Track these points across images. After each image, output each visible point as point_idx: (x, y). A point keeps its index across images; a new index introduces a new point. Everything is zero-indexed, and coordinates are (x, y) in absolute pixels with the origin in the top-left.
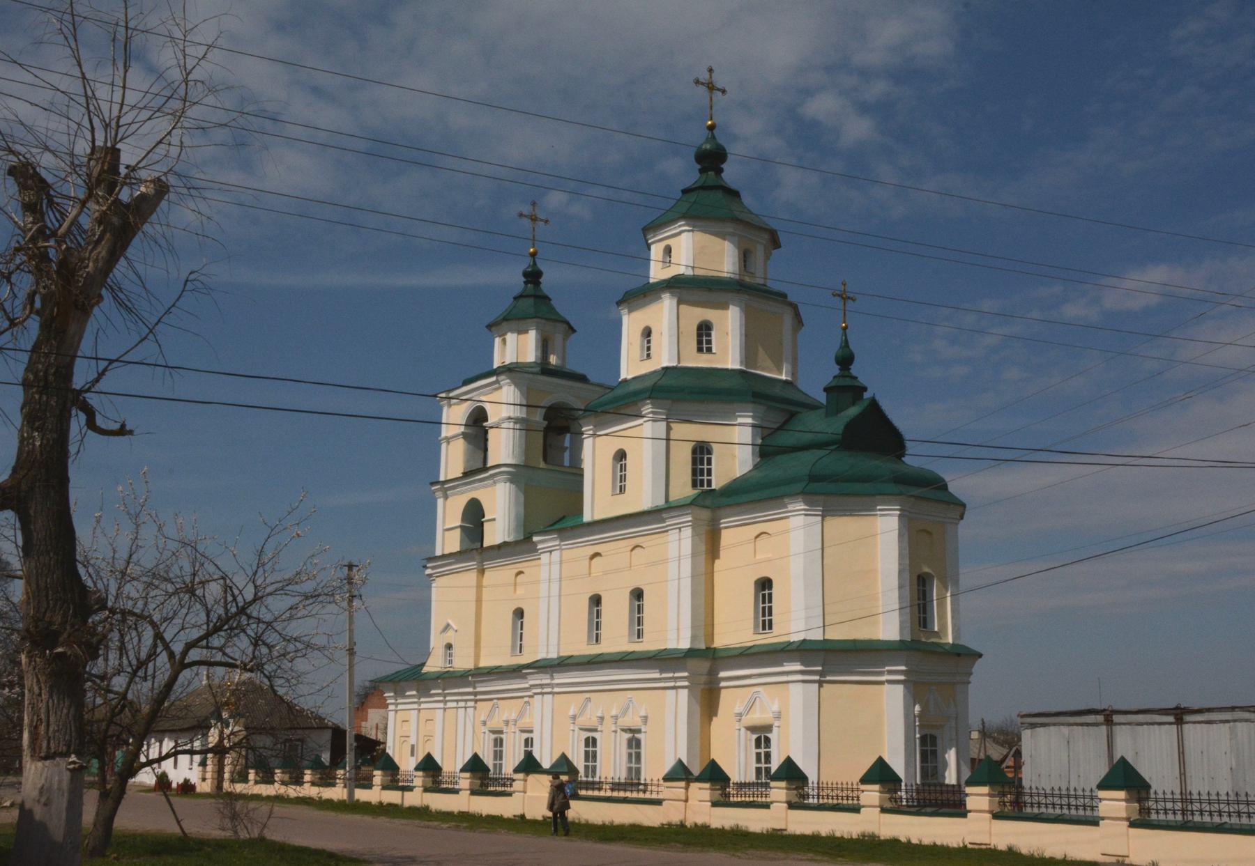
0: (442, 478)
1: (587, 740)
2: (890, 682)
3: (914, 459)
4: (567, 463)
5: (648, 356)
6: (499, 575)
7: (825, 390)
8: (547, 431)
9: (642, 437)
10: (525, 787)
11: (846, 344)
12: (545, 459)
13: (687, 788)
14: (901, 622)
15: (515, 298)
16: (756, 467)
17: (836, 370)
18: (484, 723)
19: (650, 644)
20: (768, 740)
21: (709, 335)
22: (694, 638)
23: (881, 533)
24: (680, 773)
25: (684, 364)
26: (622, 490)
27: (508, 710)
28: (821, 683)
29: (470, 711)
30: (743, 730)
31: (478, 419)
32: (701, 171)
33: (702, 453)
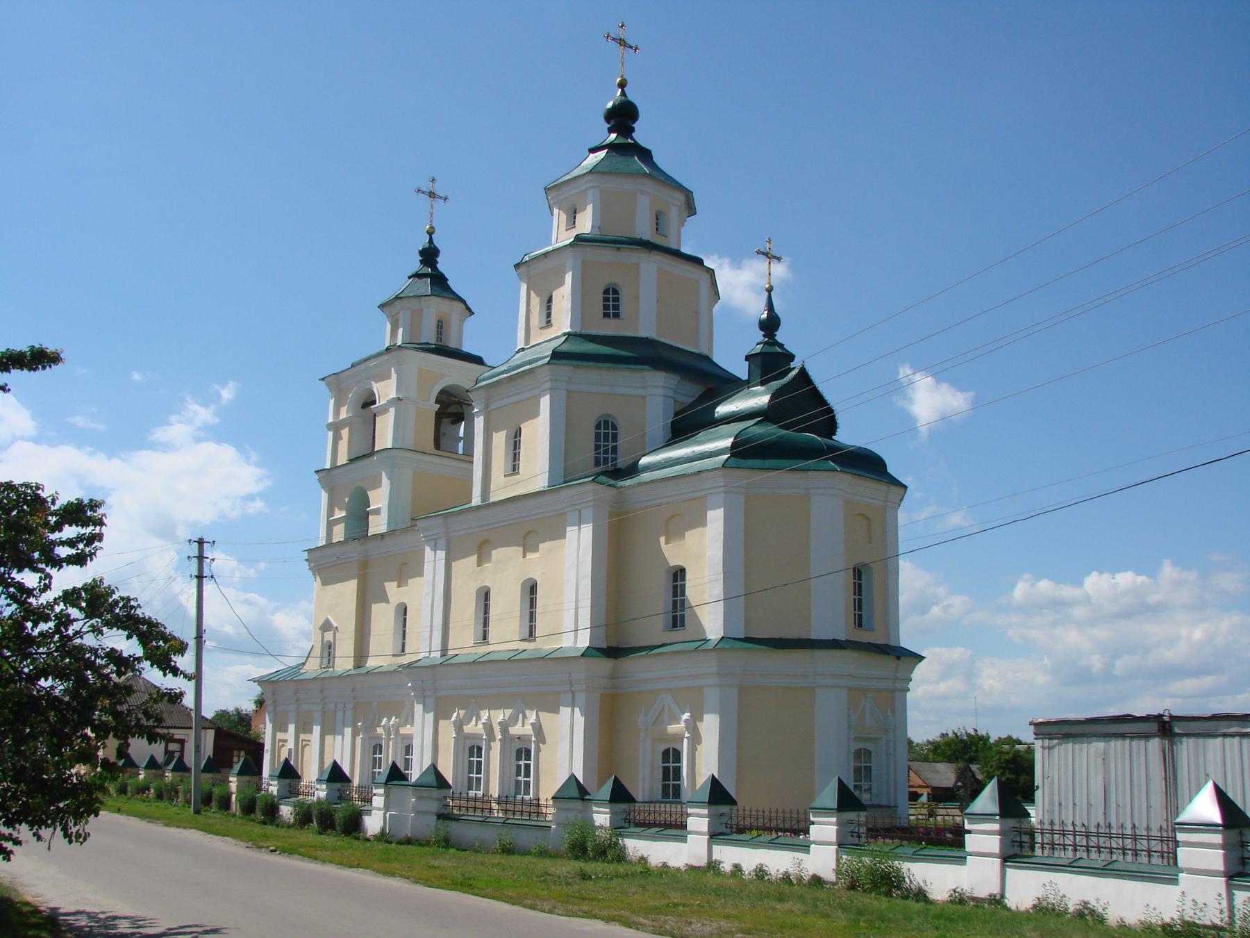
3: (846, 436)
4: (461, 452)
7: (748, 358)
8: (439, 416)
17: (760, 336)
33: (606, 428)
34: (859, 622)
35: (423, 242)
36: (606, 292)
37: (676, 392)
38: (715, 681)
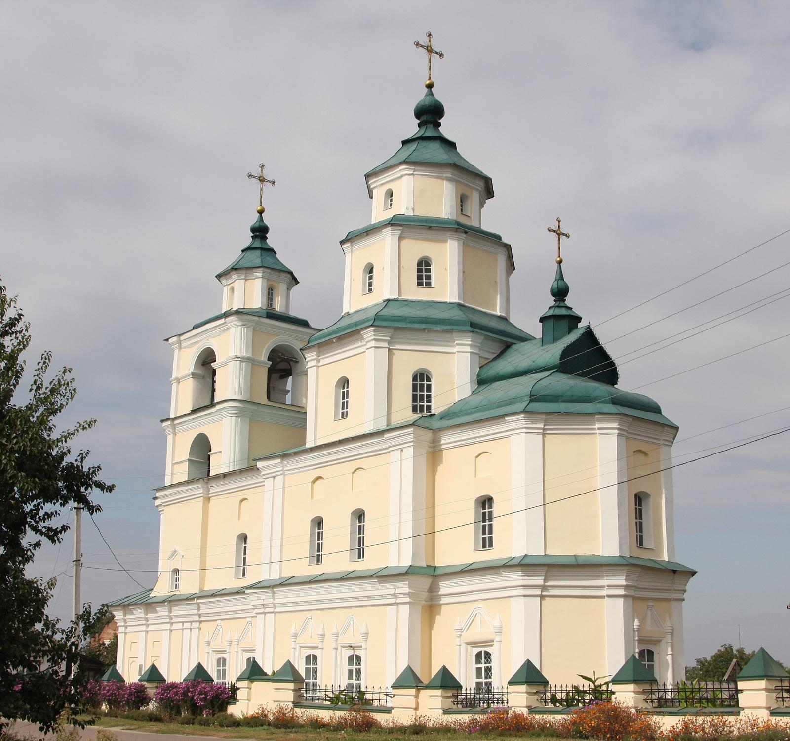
0: (172, 416)
1: (308, 657)
2: (609, 596)
3: (625, 385)
5: (370, 290)
6: (224, 502)
7: (542, 320)
9: (364, 364)
10: (249, 694)
11: (561, 277)
12: (269, 397)
13: (417, 696)
14: (620, 539)
15: (243, 251)
16: (473, 393)
17: (551, 301)
18: (209, 644)
19: (371, 562)
20: (488, 655)
21: (429, 271)
22: (415, 556)
23: (599, 447)
24: (409, 680)
25: (405, 297)
26: (344, 416)
27: (231, 630)
28: (542, 597)
29: (195, 632)
30: (463, 645)
31: (207, 359)
32: (420, 125)
34: (640, 542)
35: (254, 219)
36: (420, 264)
37: (480, 349)
38: (622, 592)
